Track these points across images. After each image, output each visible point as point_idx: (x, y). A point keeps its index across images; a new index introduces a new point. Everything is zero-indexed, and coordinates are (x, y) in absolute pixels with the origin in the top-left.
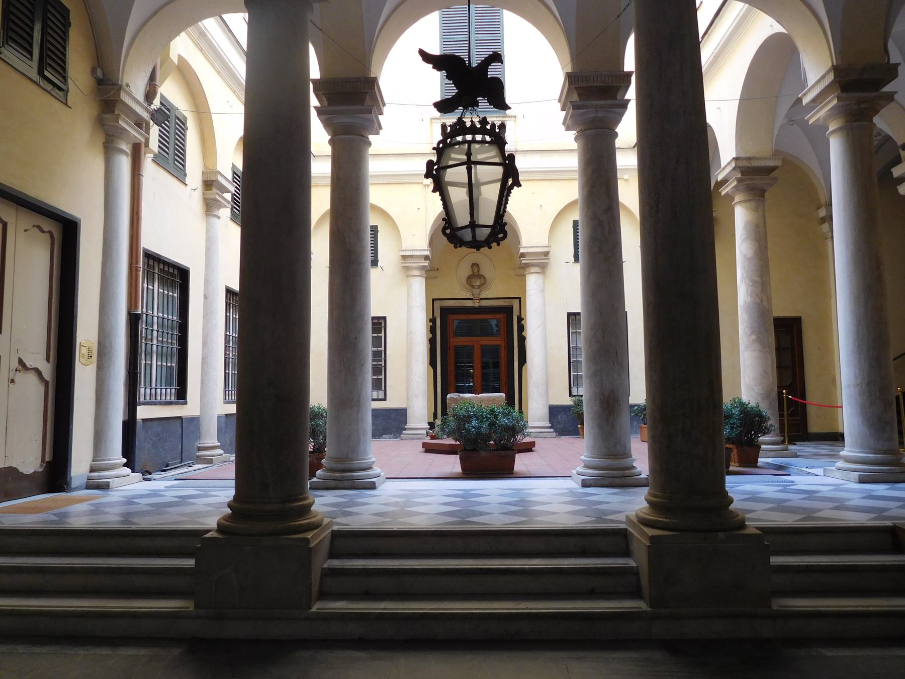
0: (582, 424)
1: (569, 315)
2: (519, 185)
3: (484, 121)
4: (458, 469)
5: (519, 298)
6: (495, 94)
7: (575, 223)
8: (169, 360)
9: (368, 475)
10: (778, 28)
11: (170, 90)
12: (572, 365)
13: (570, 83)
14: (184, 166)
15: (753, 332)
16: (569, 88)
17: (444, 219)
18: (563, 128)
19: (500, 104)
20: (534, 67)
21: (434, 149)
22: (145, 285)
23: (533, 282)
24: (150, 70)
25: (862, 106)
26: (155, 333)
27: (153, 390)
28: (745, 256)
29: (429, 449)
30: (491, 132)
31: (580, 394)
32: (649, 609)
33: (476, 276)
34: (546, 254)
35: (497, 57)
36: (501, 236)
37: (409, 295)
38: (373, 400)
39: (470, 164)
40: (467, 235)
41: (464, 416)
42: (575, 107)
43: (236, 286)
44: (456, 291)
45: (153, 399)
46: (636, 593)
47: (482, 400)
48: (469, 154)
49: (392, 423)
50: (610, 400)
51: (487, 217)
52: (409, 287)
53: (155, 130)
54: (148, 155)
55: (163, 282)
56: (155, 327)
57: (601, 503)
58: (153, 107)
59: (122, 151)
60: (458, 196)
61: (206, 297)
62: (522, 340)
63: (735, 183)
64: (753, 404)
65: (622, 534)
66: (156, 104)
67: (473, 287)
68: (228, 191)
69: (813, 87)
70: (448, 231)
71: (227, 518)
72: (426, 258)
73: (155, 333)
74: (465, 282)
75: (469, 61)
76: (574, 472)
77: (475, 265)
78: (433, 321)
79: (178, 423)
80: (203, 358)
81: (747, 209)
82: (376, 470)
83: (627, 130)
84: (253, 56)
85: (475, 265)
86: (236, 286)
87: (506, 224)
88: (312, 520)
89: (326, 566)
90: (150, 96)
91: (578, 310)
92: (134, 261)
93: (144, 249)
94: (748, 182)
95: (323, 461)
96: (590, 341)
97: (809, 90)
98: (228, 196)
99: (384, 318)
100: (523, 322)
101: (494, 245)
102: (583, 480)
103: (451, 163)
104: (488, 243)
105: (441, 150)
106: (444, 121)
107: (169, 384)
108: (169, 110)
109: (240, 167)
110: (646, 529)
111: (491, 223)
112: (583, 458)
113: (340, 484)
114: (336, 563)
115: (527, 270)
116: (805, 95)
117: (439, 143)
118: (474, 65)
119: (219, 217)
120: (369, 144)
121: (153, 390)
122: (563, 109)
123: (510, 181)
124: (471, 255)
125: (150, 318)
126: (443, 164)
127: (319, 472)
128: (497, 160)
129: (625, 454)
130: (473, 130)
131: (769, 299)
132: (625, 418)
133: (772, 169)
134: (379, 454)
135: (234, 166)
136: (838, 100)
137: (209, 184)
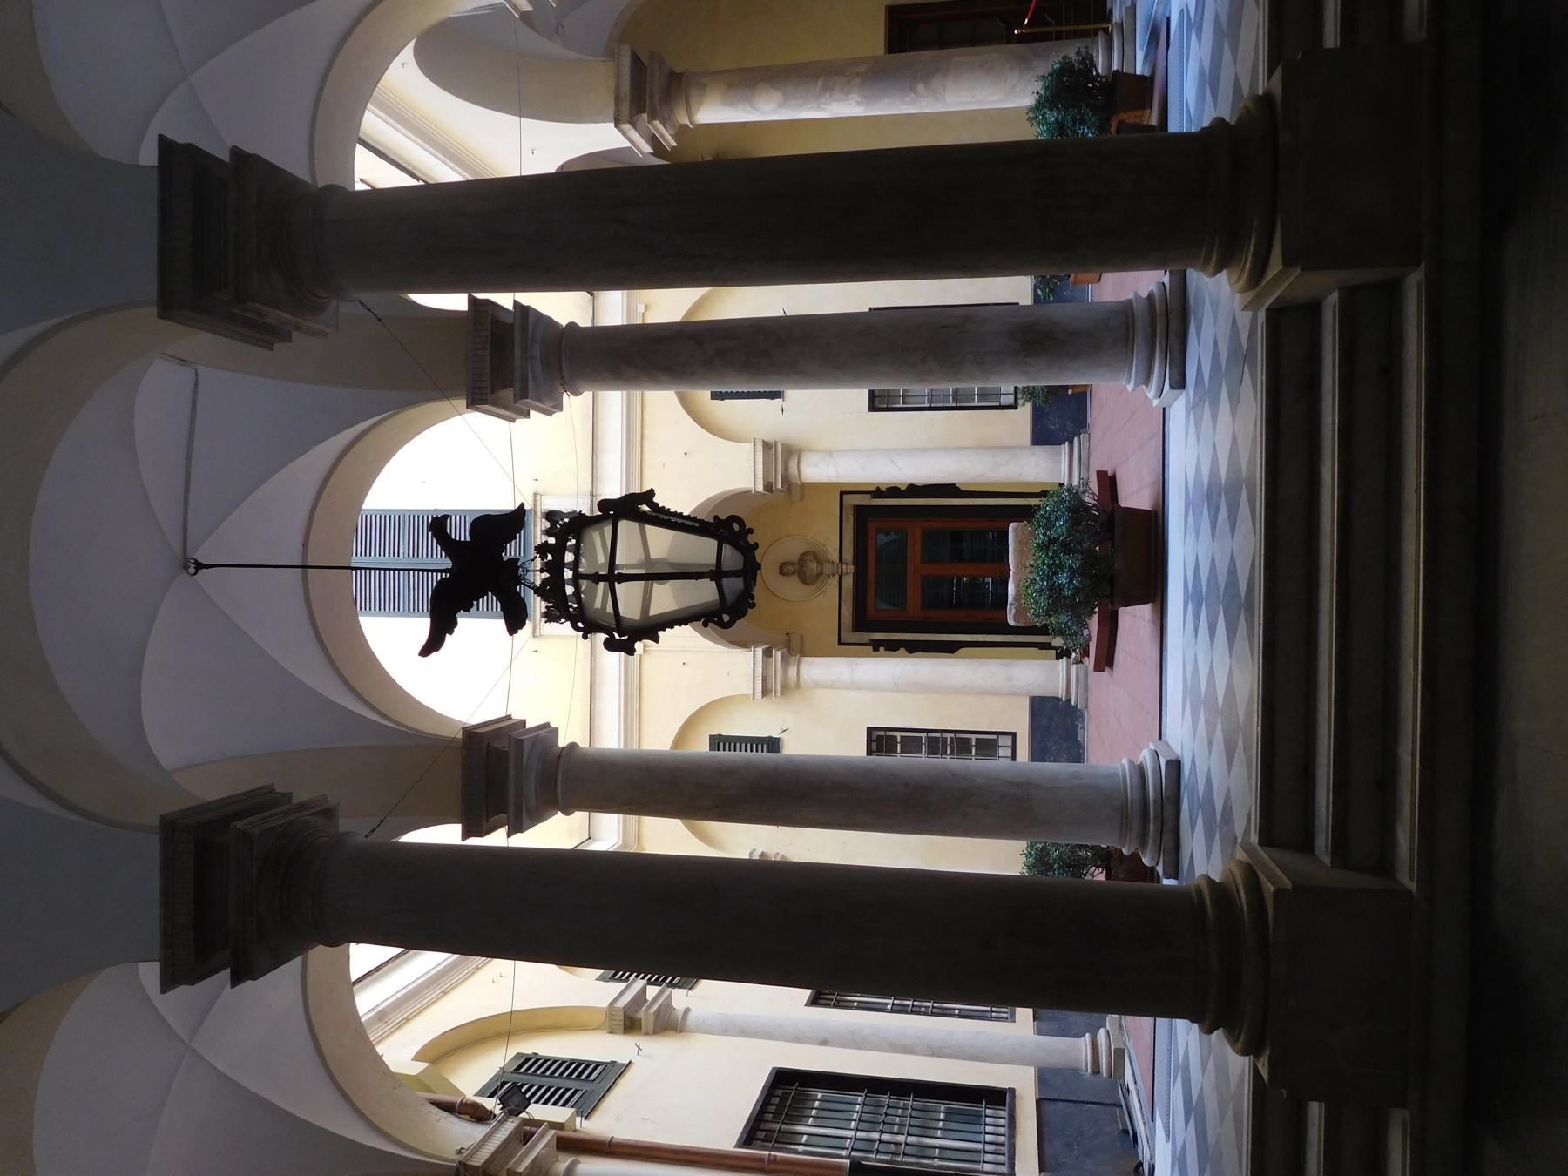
0: (1067, 387)
1: (873, 408)
2: (651, 493)
3: (542, 549)
4: (1145, 610)
5: (842, 494)
6: (498, 528)
7: (716, 396)
8: (933, 1115)
9: (1154, 772)
10: (408, 53)
11: (472, 1078)
12: (960, 404)
14: (598, 1065)
15: (913, 89)
16: (493, 404)
17: (705, 625)
18: (557, 415)
19: (515, 520)
20: (455, 463)
21: (585, 637)
22: (801, 1148)
23: (814, 470)
24: (436, 1110)
26: (885, 1137)
27: (989, 1148)
28: (780, 105)
29: (1106, 660)
31: (1012, 390)
32: (1423, 267)
33: (803, 569)
34: (767, 446)
35: (438, 525)
36: (736, 526)
37: (832, 686)
38: (1014, 757)
39: (613, 577)
40: (734, 585)
41: (1050, 597)
42: (523, 394)
43: (806, 993)
44: (825, 604)
45: (1004, 1149)
46: (1391, 292)
47: (1019, 564)
48: (596, 578)
49: (1056, 723)
50: (1026, 338)
51: (703, 550)
52: (817, 685)
53: (536, 1111)
54: (578, 1126)
55: (796, 1116)
56: (875, 1136)
57: (1216, 355)
58: (497, 1111)
60: (665, 598)
61: (824, 1042)
62: (914, 490)
63: (658, 123)
64: (1038, 87)
65: (1276, 317)
66: (491, 1104)
67: (820, 574)
68: (644, 990)
70: (726, 618)
71: (1233, 1039)
72: (767, 654)
73: (885, 1137)
75: (441, 571)
76: (1156, 402)
77: (783, 569)
78: (876, 646)
79: (1046, 1106)
80: (933, 1055)
81: (701, 103)
82: (1145, 756)
83: (563, 307)
85: (783, 569)
86: (806, 993)
87: (716, 517)
88: (1240, 881)
89: (1327, 860)
90: (478, 1115)
91: (865, 393)
92: (758, 1165)
93: (737, 1146)
94: (656, 100)
95: (1125, 852)
96: (922, 376)
98: (652, 991)
99: (870, 730)
101: (751, 539)
102: (1172, 387)
103: (610, 609)
104: (748, 550)
105: (587, 624)
107: (976, 1118)
108: (504, 1083)
109: (600, 972)
110: (1270, 274)
111: (713, 543)
112: (1130, 387)
113: (1169, 825)
114: (1322, 840)
115: (794, 479)
118: (447, 563)
119: (687, 1010)
120: (573, 746)
121: (989, 1148)
122: (527, 415)
123: (645, 508)
124: (768, 574)
125: (859, 1145)
126: (612, 622)
127: (1146, 861)
128: (608, 530)
129: (1125, 311)
130: (555, 568)
131: (857, 62)
132: (1058, 312)
134: (1115, 749)
135: (599, 979)
137: (630, 1024)
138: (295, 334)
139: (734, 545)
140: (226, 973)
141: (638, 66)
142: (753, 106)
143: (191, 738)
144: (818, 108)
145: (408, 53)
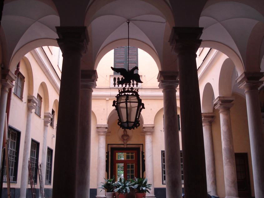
2: (144, 108)
5: (143, 144)
6: (138, 79)
10: (228, 57)
11: (22, 70)
12: (164, 172)
13: (161, 74)
16: (160, 77)
20: (148, 66)
21: (116, 97)
23: (148, 139)
25: (254, 85)
28: (224, 131)
30: (135, 92)
33: (125, 137)
34: (153, 127)
35: (137, 68)
36: (138, 125)
39: (126, 102)
40: (126, 125)
42: (162, 82)
44: (117, 141)
51: (133, 119)
59: (6, 91)
60: (124, 112)
62: (144, 161)
67: (124, 140)
69: (239, 77)
70: (120, 124)
72: (106, 128)
74: (121, 137)
78: (107, 153)
84: (63, 81)
87: (139, 121)
97: (215, 101)
100: (144, 154)
101: (135, 128)
104: (132, 127)
105: (118, 97)
106: (115, 76)
116: (237, 79)
117: (118, 95)
118: (130, 69)
122: (158, 81)
123: (141, 107)
131: (233, 146)
133: (232, 101)
136: (247, 83)
137: (30, 100)
138: (171, 46)
139: (133, 125)
140: (58, 38)
141: (230, 101)
142: (223, 125)
143: (96, 25)
144: (223, 139)
145: (228, 57)
